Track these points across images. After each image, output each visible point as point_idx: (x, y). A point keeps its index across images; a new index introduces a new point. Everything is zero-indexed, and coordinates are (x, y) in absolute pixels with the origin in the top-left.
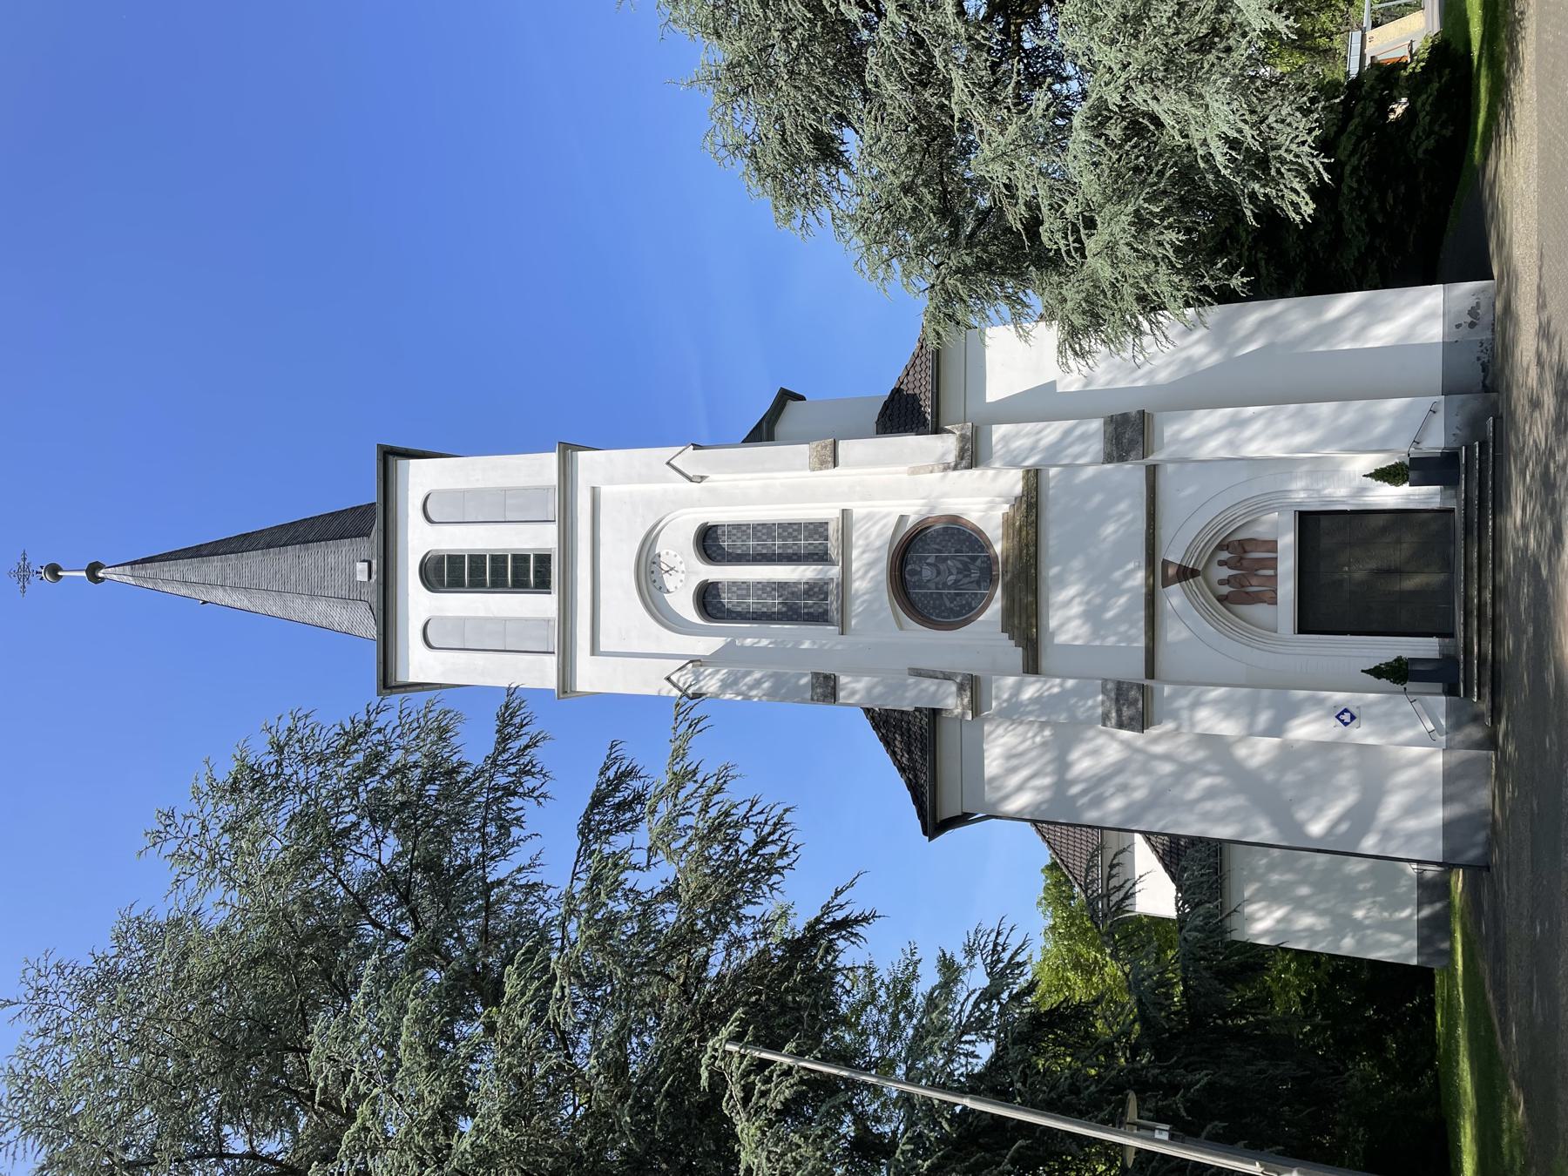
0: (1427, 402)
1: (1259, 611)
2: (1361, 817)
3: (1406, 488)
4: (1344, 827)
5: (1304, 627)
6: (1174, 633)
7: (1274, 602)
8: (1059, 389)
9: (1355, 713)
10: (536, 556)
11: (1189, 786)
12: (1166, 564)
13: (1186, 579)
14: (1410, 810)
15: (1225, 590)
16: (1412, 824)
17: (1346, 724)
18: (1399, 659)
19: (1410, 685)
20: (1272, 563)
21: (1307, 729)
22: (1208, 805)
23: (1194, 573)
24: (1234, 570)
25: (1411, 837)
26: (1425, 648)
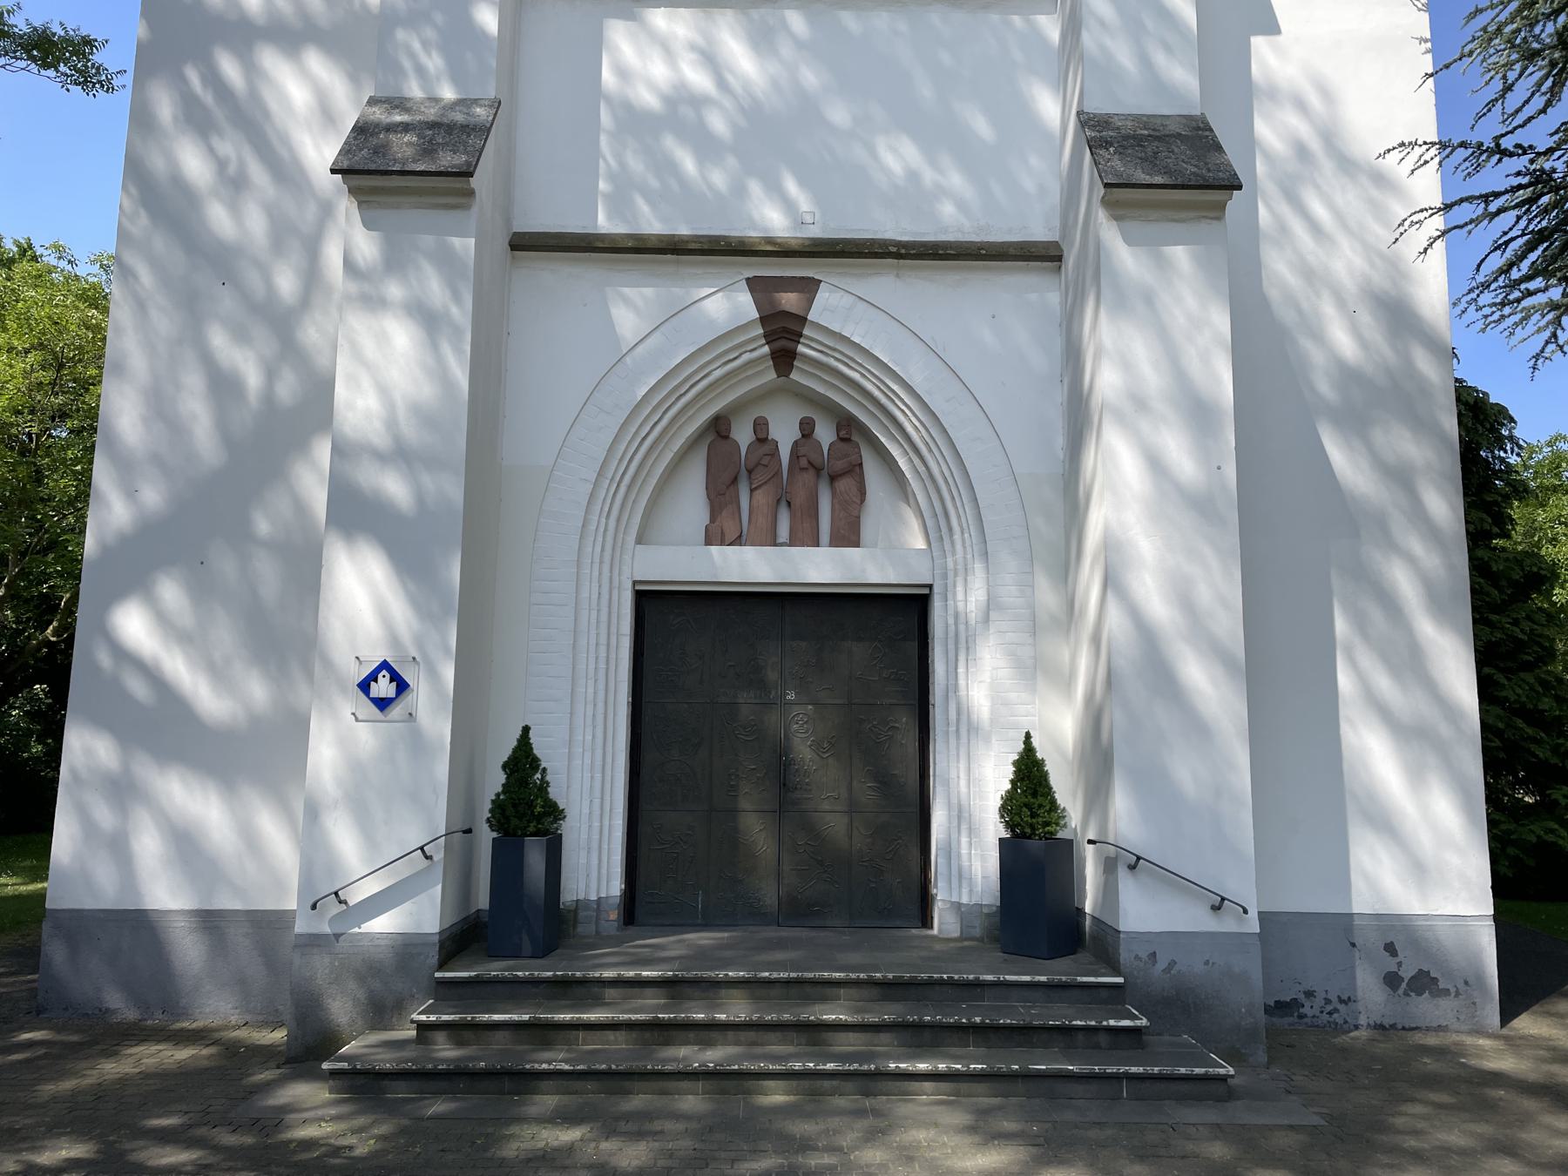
0: (1243, 888)
1: (690, 503)
2: (166, 729)
3: (993, 829)
4: (138, 688)
5: (656, 608)
6: (631, 307)
7: (713, 537)
8: (1259, 43)
9: (396, 711)
10: (903, 617)
11: (240, 335)
12: (809, 287)
13: (769, 337)
14: (186, 846)
15: (743, 435)
16: (148, 845)
17: (364, 686)
18: (554, 813)
19: (486, 837)
20: (806, 536)
21: (363, 599)
22: (194, 382)
23: (784, 358)
24: (792, 436)
25: (119, 848)
26: (594, 862)
